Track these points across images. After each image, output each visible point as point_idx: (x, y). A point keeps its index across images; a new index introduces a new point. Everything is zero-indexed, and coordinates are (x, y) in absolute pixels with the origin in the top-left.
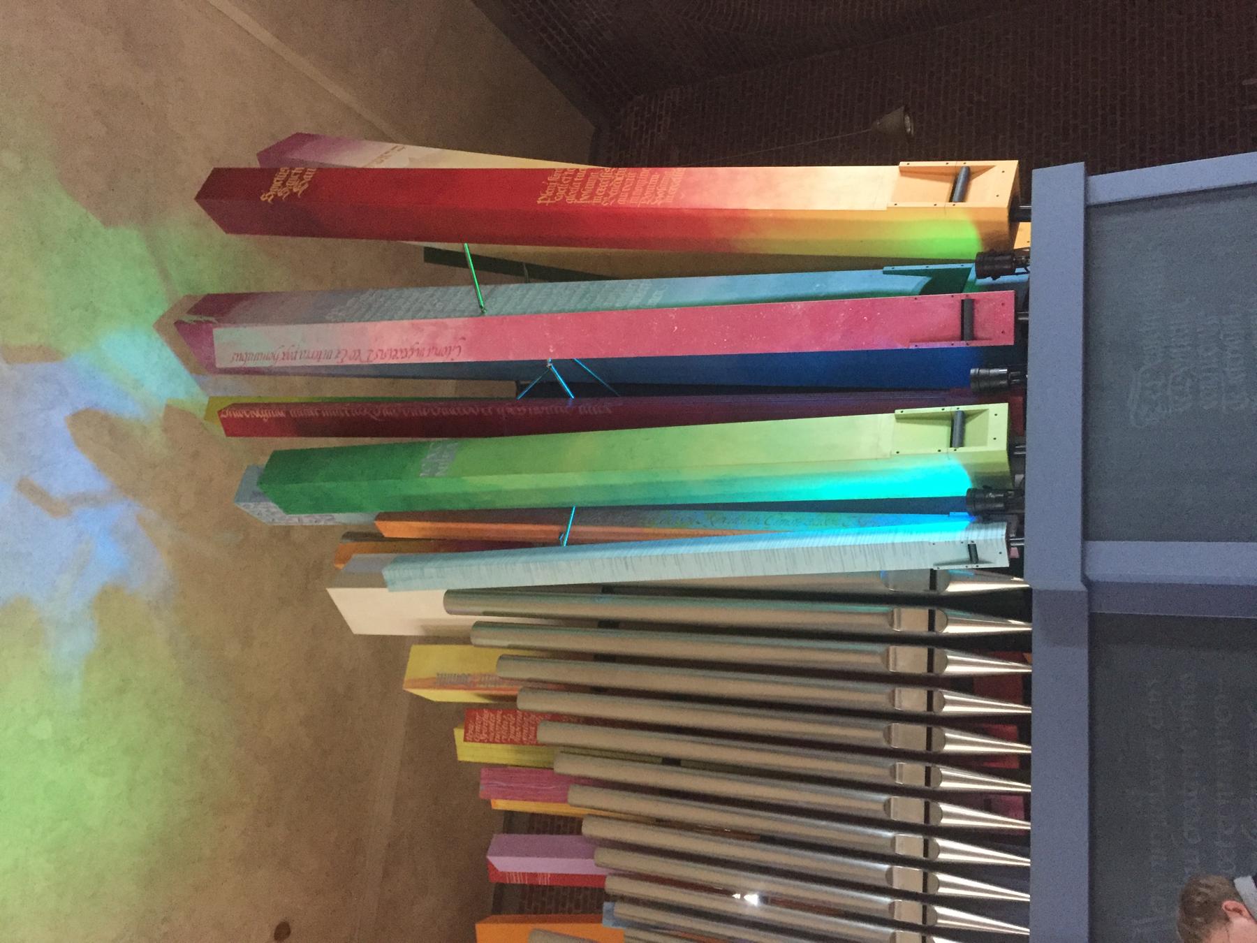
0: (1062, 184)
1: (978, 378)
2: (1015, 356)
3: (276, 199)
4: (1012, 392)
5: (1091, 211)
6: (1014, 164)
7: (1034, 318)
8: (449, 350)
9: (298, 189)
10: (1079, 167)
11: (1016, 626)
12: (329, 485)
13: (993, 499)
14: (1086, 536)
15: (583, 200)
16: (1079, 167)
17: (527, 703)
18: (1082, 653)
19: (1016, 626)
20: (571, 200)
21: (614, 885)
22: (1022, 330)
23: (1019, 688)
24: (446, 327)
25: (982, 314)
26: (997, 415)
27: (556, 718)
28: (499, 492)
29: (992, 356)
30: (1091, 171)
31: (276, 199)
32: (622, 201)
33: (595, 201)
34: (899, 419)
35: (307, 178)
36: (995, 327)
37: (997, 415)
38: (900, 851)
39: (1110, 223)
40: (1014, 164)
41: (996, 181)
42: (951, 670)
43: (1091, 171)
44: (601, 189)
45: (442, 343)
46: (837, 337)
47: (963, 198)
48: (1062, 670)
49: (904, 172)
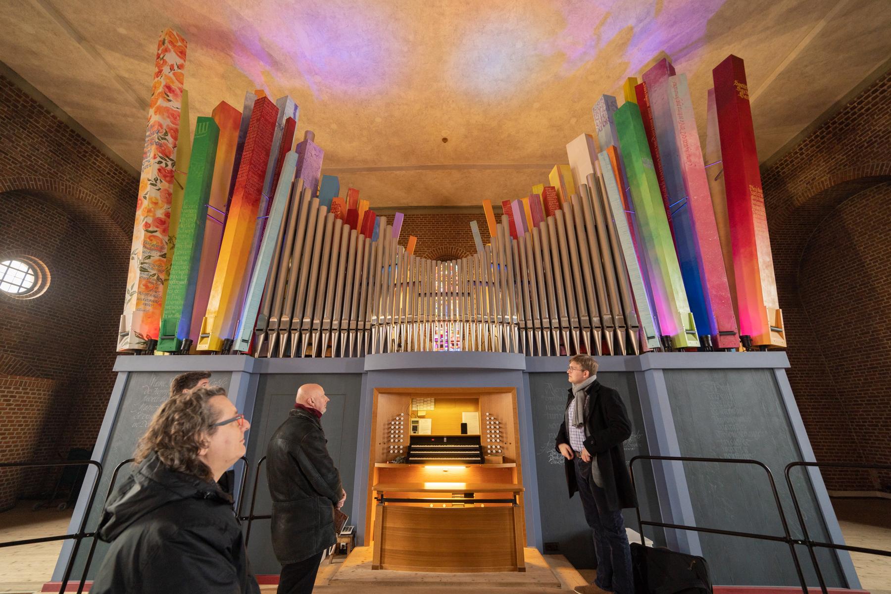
0: (781, 361)
1: (707, 337)
2: (716, 348)
3: (736, 87)
4: (703, 348)
5: (772, 370)
6: (785, 346)
7: (726, 353)
10: (788, 365)
12: (632, 127)
13: (668, 344)
14: (664, 370)
15: (753, 202)
16: (788, 365)
17: (550, 220)
18: (624, 369)
20: (752, 197)
22: (723, 350)
25: (731, 338)
26: (696, 343)
27: (548, 226)
28: (638, 186)
29: (715, 340)
30: (787, 370)
31: (736, 87)
32: (754, 216)
34: (777, 311)
36: (723, 342)
37: (696, 343)
38: (535, 321)
39: (768, 375)
40: (785, 346)
41: (779, 340)
42: (584, 333)
44: (758, 208)
46: (714, 293)
47: (772, 330)
49: (777, 311)
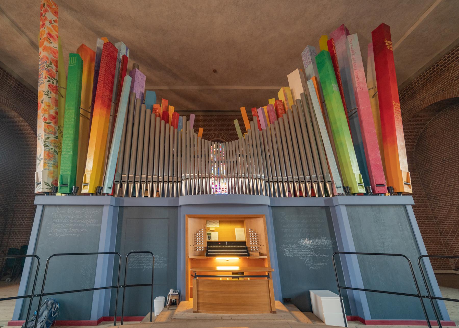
0: (410, 201)
1: (369, 188)
2: (374, 194)
3: (385, 42)
5: (405, 206)
8: (360, 86)
9: (388, 47)
10: (413, 203)
11: (166, 196)
19: (166, 196)
20: (394, 108)
21: (280, 119)
22: (378, 194)
23: (314, 196)
24: (365, 85)
29: (373, 190)
30: (413, 206)
32: (395, 119)
33: (395, 113)
35: (391, 49)
36: (378, 190)
39: (402, 208)
40: (412, 192)
43: (413, 206)
44: (397, 114)
45: (361, 85)
48: (320, 202)
